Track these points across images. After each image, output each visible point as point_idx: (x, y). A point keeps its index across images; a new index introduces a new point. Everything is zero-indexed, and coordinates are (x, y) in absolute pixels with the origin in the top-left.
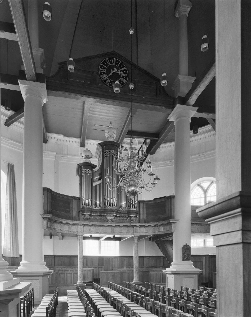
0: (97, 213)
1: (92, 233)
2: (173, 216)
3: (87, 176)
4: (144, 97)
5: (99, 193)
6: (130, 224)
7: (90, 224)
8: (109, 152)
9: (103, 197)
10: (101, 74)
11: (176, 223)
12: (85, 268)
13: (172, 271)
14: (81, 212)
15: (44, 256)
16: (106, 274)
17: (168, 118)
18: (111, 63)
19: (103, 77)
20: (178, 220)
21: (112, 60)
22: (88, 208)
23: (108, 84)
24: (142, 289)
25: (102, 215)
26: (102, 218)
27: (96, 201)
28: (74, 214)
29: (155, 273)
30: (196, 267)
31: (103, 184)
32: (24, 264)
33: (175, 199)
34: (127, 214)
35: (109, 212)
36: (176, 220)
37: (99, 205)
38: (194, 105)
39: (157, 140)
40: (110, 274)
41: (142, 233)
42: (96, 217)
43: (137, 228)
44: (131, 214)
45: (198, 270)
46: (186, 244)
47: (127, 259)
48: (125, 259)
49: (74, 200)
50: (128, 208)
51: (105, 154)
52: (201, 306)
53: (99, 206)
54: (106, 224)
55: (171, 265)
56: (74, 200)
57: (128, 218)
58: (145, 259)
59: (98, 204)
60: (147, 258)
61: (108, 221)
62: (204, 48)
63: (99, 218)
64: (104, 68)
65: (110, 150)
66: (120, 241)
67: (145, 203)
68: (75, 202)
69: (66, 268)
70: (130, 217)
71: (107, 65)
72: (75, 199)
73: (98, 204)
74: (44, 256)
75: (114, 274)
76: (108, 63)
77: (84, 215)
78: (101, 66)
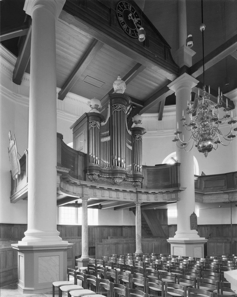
0: (105, 174)
1: (97, 196)
2: (179, 184)
3: (96, 128)
4: (156, 56)
5: (103, 152)
6: (137, 189)
7: (98, 187)
8: (119, 107)
9: (111, 157)
10: (119, 16)
11: (183, 191)
12: (69, 239)
13: (185, 241)
14: (88, 171)
15: (57, 225)
16: (102, 245)
17: (168, 86)
18: (127, 7)
19: (120, 20)
20: (186, 188)
21: (129, 6)
22: (97, 167)
23: (125, 29)
24: (155, 260)
25: (110, 177)
26: (111, 181)
27: (106, 161)
28: (80, 172)
29: (147, 243)
30: (201, 236)
31: (111, 141)
32: (32, 235)
33: (180, 166)
34: (132, 179)
35: (119, 174)
36: (183, 188)
37: (105, 165)
38: (197, 78)
39: (142, 108)
40: (105, 245)
41: (144, 200)
42: (103, 179)
43: (157, 195)
44: (138, 178)
45: (204, 239)
46: (194, 213)
47: (106, 229)
48: (104, 228)
49: (79, 155)
50: (133, 172)
51: (115, 107)
52: (151, 274)
53: (107, 166)
54: (114, 188)
55: (24, 236)
56: (79, 155)
57: (133, 183)
58: (124, 229)
59: (107, 165)
60: (125, 227)
61: (115, 184)
62: (141, 39)
63: (106, 180)
64: (122, 11)
65: (121, 105)
66: (100, 210)
67: (147, 168)
68: (80, 158)
69: (155, 241)
70: (136, 182)
71: (124, 8)
72: (81, 155)
73: (107, 165)
74: (57, 225)
75: (109, 245)
76: (124, 6)
77: (92, 175)
78: (119, 7)
